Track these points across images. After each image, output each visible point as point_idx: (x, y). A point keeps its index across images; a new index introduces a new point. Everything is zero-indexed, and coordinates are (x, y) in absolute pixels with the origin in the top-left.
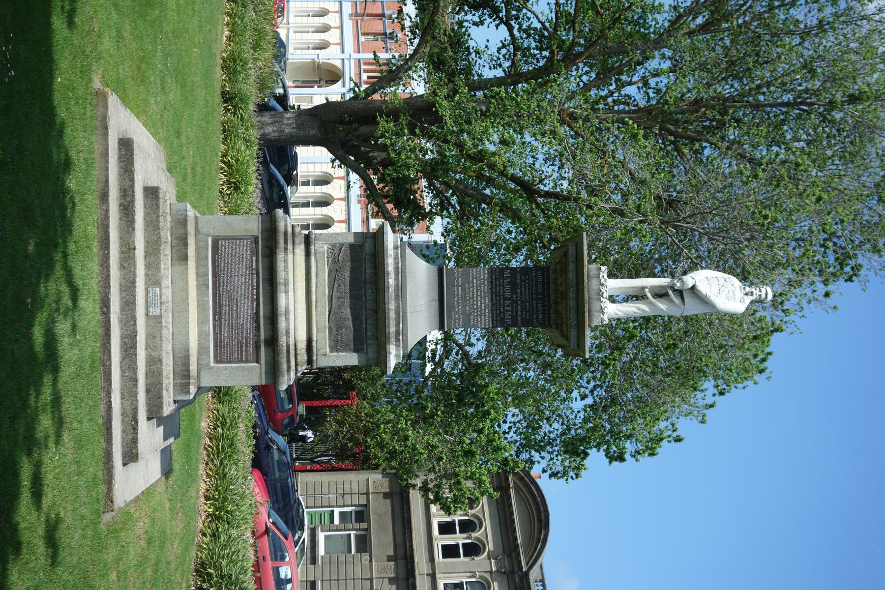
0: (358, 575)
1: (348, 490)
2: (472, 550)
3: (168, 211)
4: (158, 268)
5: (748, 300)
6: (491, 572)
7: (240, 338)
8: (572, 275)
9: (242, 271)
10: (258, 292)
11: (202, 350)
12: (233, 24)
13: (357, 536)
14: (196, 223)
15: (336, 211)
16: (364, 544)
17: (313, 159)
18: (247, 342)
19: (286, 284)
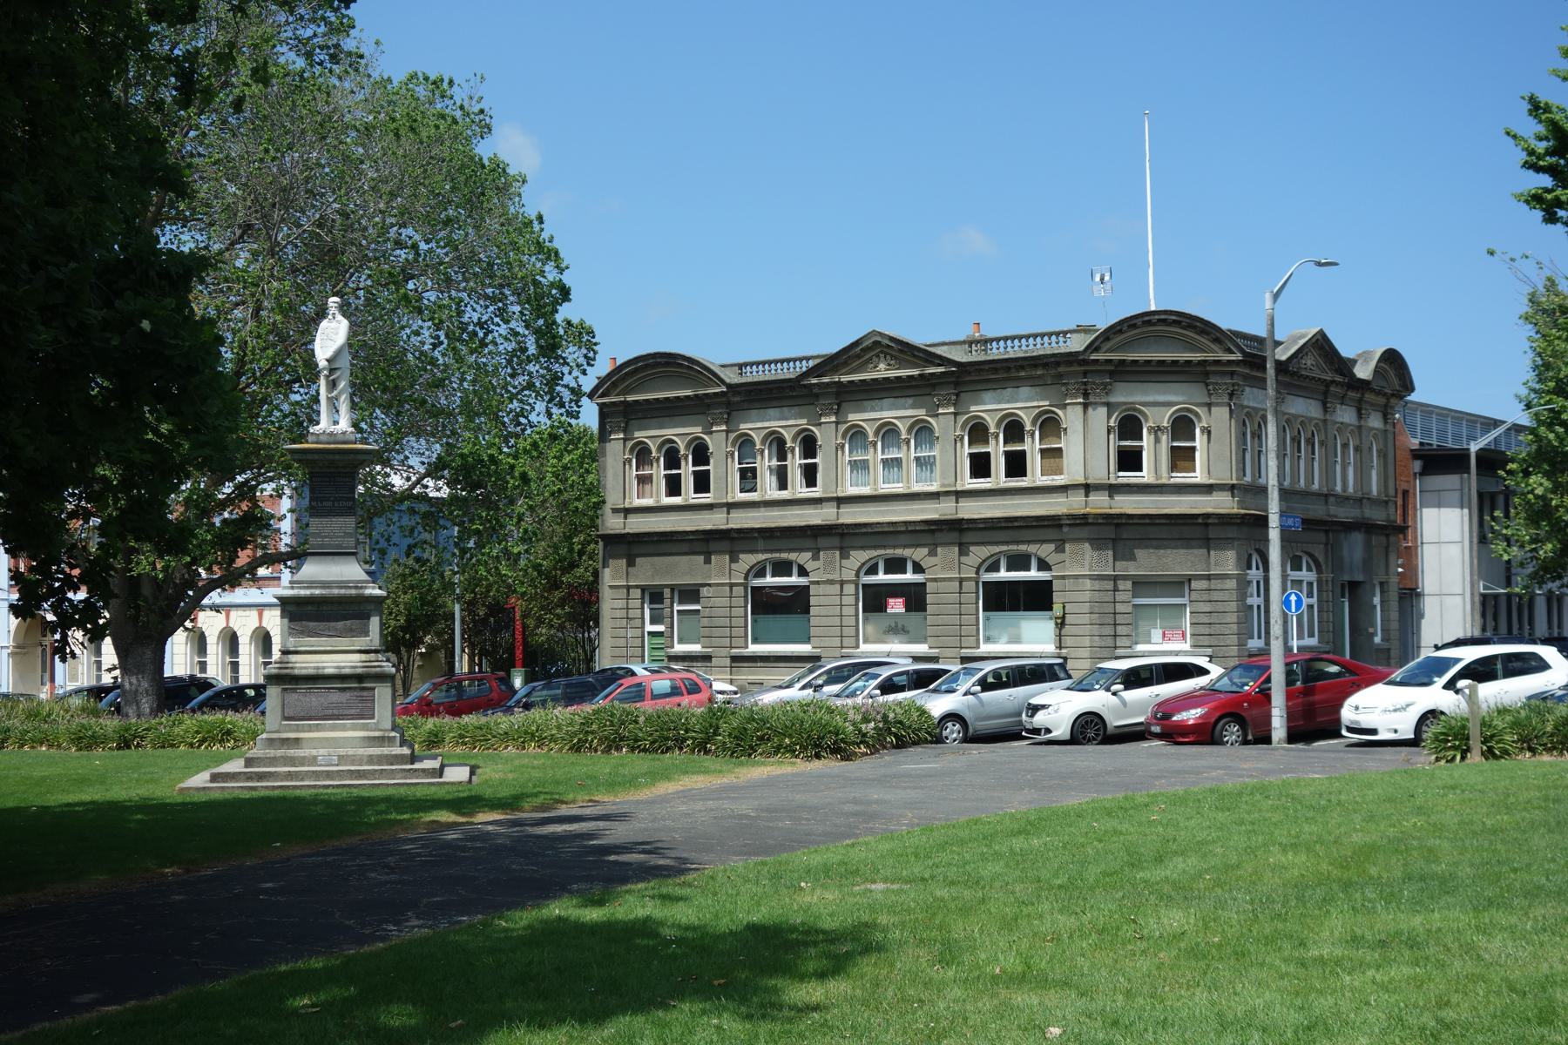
0: (726, 601)
1: (623, 613)
2: (701, 454)
5: (339, 317)
6: (727, 432)
8: (316, 457)
11: (365, 728)
13: (680, 603)
15: (245, 624)
16: (690, 594)
17: (178, 659)
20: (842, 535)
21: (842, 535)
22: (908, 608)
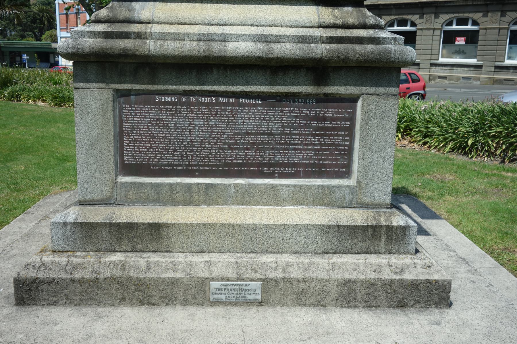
3: (62, 260)
4: (173, 283)
7: (308, 131)
9: (182, 122)
10: (224, 94)
11: (325, 199)
12: (34, 97)
14: (92, 203)
18: (317, 119)
19: (209, 38)
20: (437, 7)
21: (437, 7)
22: (467, 42)
